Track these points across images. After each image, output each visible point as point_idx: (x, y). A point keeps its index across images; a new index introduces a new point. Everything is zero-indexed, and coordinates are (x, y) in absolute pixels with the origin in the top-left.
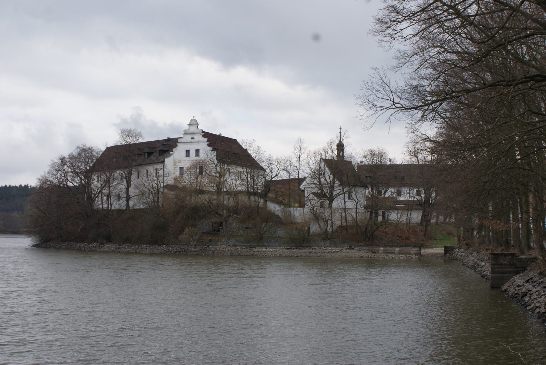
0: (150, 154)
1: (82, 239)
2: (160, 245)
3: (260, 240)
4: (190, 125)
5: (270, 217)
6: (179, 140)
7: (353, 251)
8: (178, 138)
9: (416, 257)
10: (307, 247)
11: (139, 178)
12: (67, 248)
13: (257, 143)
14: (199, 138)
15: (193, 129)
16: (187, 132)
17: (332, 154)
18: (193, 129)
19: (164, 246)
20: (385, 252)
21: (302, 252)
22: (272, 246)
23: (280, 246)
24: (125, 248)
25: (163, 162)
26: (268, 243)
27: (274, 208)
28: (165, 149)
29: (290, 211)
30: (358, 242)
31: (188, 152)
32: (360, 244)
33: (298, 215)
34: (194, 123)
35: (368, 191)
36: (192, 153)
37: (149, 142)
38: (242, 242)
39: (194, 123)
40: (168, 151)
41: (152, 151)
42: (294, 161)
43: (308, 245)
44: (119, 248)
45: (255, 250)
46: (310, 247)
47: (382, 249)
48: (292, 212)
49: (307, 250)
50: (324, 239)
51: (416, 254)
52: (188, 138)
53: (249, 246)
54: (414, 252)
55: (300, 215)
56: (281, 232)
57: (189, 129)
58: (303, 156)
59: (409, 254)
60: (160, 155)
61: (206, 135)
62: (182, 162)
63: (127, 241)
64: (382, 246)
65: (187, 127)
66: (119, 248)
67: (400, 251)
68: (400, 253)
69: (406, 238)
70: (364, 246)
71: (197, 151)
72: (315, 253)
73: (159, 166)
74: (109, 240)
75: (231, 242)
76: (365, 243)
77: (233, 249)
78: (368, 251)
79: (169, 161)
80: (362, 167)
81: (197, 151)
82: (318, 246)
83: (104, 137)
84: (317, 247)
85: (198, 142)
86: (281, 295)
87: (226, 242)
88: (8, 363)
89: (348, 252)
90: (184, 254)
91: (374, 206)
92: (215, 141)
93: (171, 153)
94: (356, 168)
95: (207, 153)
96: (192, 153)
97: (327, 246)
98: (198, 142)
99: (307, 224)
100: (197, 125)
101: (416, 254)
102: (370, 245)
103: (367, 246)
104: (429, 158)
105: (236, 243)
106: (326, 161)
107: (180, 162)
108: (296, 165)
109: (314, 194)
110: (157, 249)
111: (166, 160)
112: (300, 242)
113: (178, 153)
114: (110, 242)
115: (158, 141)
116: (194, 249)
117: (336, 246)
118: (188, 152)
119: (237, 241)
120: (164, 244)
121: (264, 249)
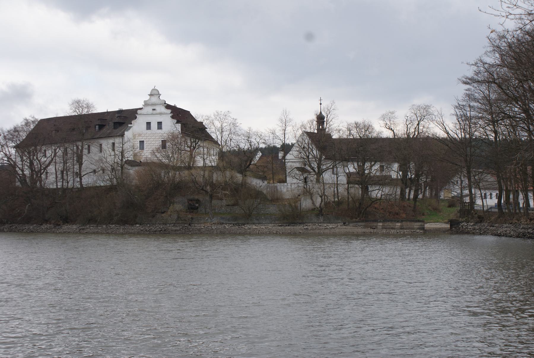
0: (101, 127)
1: (28, 220)
2: (132, 225)
3: (249, 217)
4: (151, 95)
5: (258, 194)
6: (139, 112)
7: (347, 227)
8: (137, 109)
9: (421, 231)
10: (300, 223)
11: (101, 152)
12: (11, 231)
13: (233, 116)
14: (163, 109)
15: (154, 99)
16: (148, 103)
17: (313, 129)
18: (154, 99)
19: (138, 225)
20: (384, 228)
21: (298, 228)
22: (262, 223)
23: (272, 223)
24: (92, 228)
25: (122, 135)
26: (257, 220)
27: (256, 183)
28: (122, 121)
29: (276, 187)
30: (352, 218)
31: (149, 124)
32: (354, 220)
33: (285, 190)
34: (155, 93)
35: (352, 168)
36: (154, 126)
37: (108, 113)
38: (229, 220)
39: (155, 93)
40: (123, 123)
41: (104, 124)
42: (279, 133)
43: (301, 221)
44: (83, 229)
45: (246, 228)
46: (303, 223)
47: (381, 224)
48: (279, 188)
49: (301, 227)
50: (317, 215)
51: (419, 229)
52: (149, 109)
53: (236, 224)
54: (418, 227)
55: (287, 191)
56: (272, 209)
57: (150, 99)
58: (289, 129)
59: (413, 229)
60: (115, 128)
61: (168, 107)
62: (143, 135)
63: (92, 220)
64: (380, 222)
65: (148, 98)
66: (83, 229)
67: (401, 226)
68: (401, 229)
69: (397, 214)
70: (359, 222)
71: (160, 124)
72: (311, 230)
73: (117, 140)
74: (66, 220)
75: (215, 220)
76: (360, 219)
77: (220, 227)
78: (366, 227)
79: (128, 134)
80: (341, 140)
81: (160, 124)
82: (312, 223)
83: (58, 106)
84: (310, 224)
85: (161, 114)
86: (255, 273)
87: (209, 220)
88: (34, 356)
89: (345, 228)
90: (164, 233)
91: (362, 180)
92: (180, 115)
93: (129, 125)
94: (482, 131)
95: (171, 126)
96: (154, 126)
97: (321, 223)
98: (161, 114)
99: (297, 199)
100: (159, 95)
101: (419, 229)
102: (366, 221)
103: (363, 221)
104: (150, 156)
105: (222, 221)
106: (310, 135)
107: (140, 135)
108: (281, 138)
109: (298, 169)
110: (129, 228)
111: (126, 133)
112: (293, 220)
113: (137, 127)
114: (67, 222)
115: (107, 112)
116: (174, 228)
117: (330, 222)
118: (149, 124)
119: (223, 218)
120: (137, 224)
121: (254, 227)
